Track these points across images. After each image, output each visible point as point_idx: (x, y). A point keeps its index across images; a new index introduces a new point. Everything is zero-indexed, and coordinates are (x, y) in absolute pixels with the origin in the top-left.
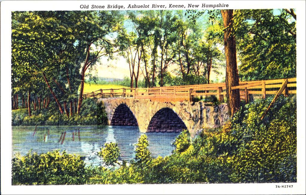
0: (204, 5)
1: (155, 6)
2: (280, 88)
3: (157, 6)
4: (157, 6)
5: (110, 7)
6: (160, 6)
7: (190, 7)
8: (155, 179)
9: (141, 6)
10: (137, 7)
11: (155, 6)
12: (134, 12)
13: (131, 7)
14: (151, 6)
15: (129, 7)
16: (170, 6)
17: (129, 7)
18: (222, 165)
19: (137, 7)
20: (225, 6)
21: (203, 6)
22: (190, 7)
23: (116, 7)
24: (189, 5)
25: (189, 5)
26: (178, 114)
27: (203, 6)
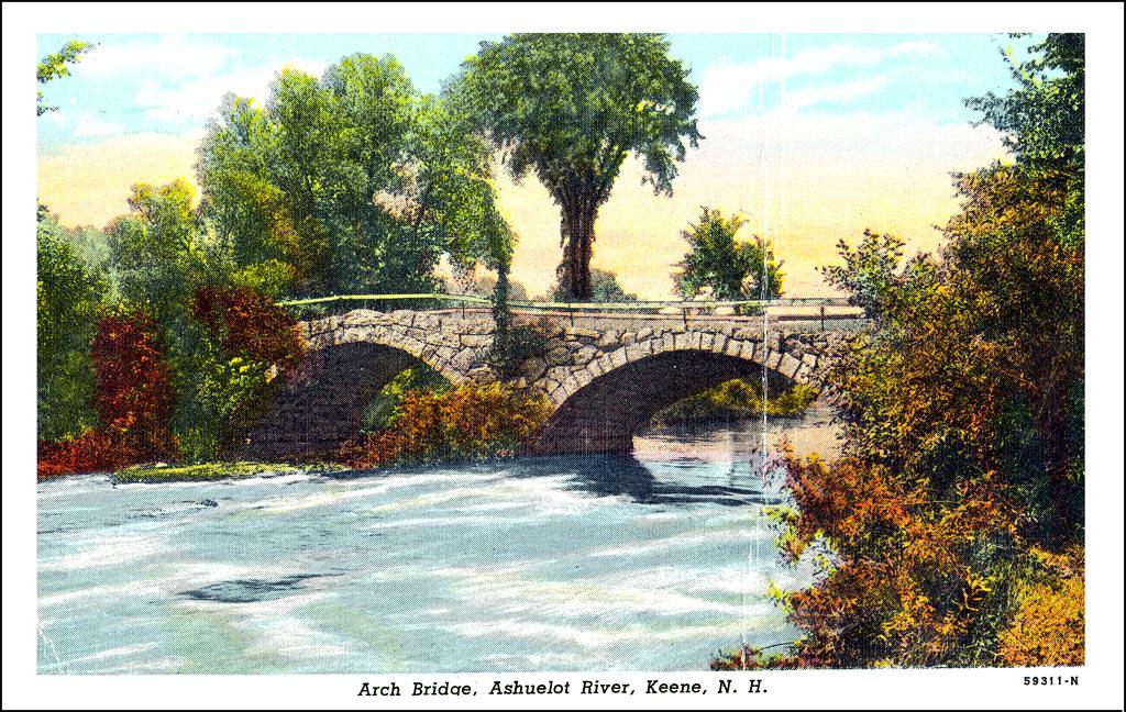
0: (756, 683)
1: (593, 689)
2: (309, 612)
3: (600, 689)
4: (600, 689)
5: (424, 690)
6: (610, 688)
7: (727, 691)
8: (777, 416)
9: (541, 689)
10: (524, 689)
11: (593, 689)
12: (82, 240)
13: (372, 692)
14: (576, 687)
15: (496, 692)
16: (650, 687)
17: (496, 692)
18: (745, 281)
19: (524, 689)
20: (378, 691)
21: (755, 689)
22: (727, 691)
23: (443, 690)
24: (722, 682)
25: (722, 682)
26: (1021, 88)
27: (755, 689)
